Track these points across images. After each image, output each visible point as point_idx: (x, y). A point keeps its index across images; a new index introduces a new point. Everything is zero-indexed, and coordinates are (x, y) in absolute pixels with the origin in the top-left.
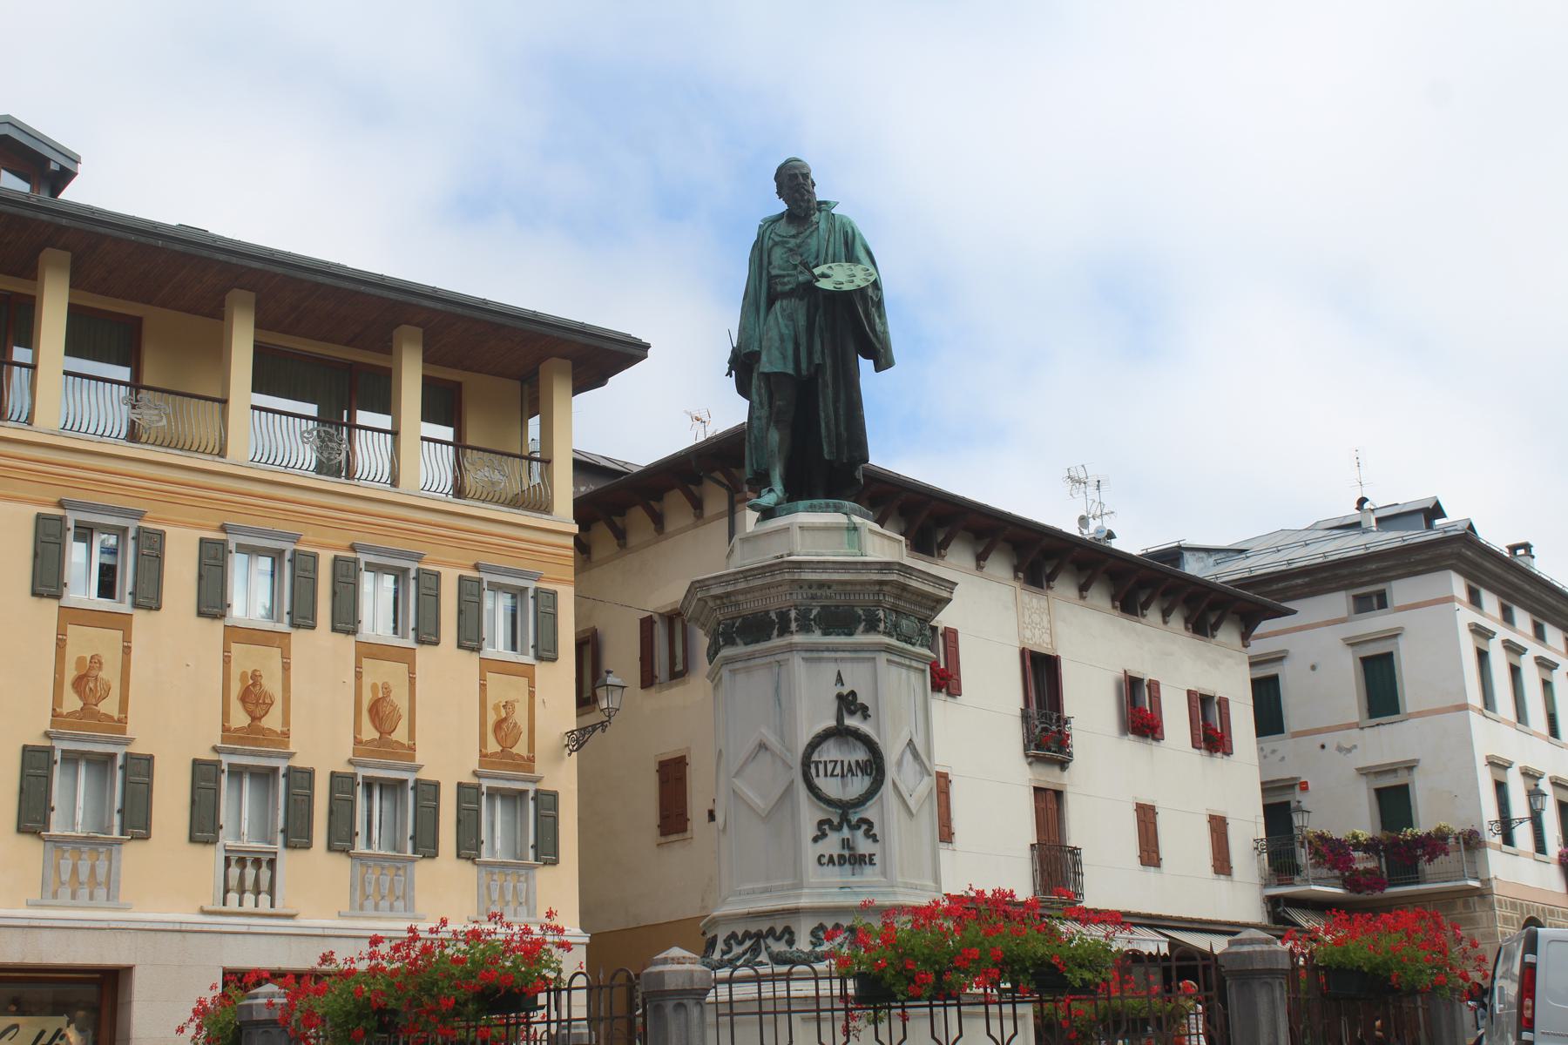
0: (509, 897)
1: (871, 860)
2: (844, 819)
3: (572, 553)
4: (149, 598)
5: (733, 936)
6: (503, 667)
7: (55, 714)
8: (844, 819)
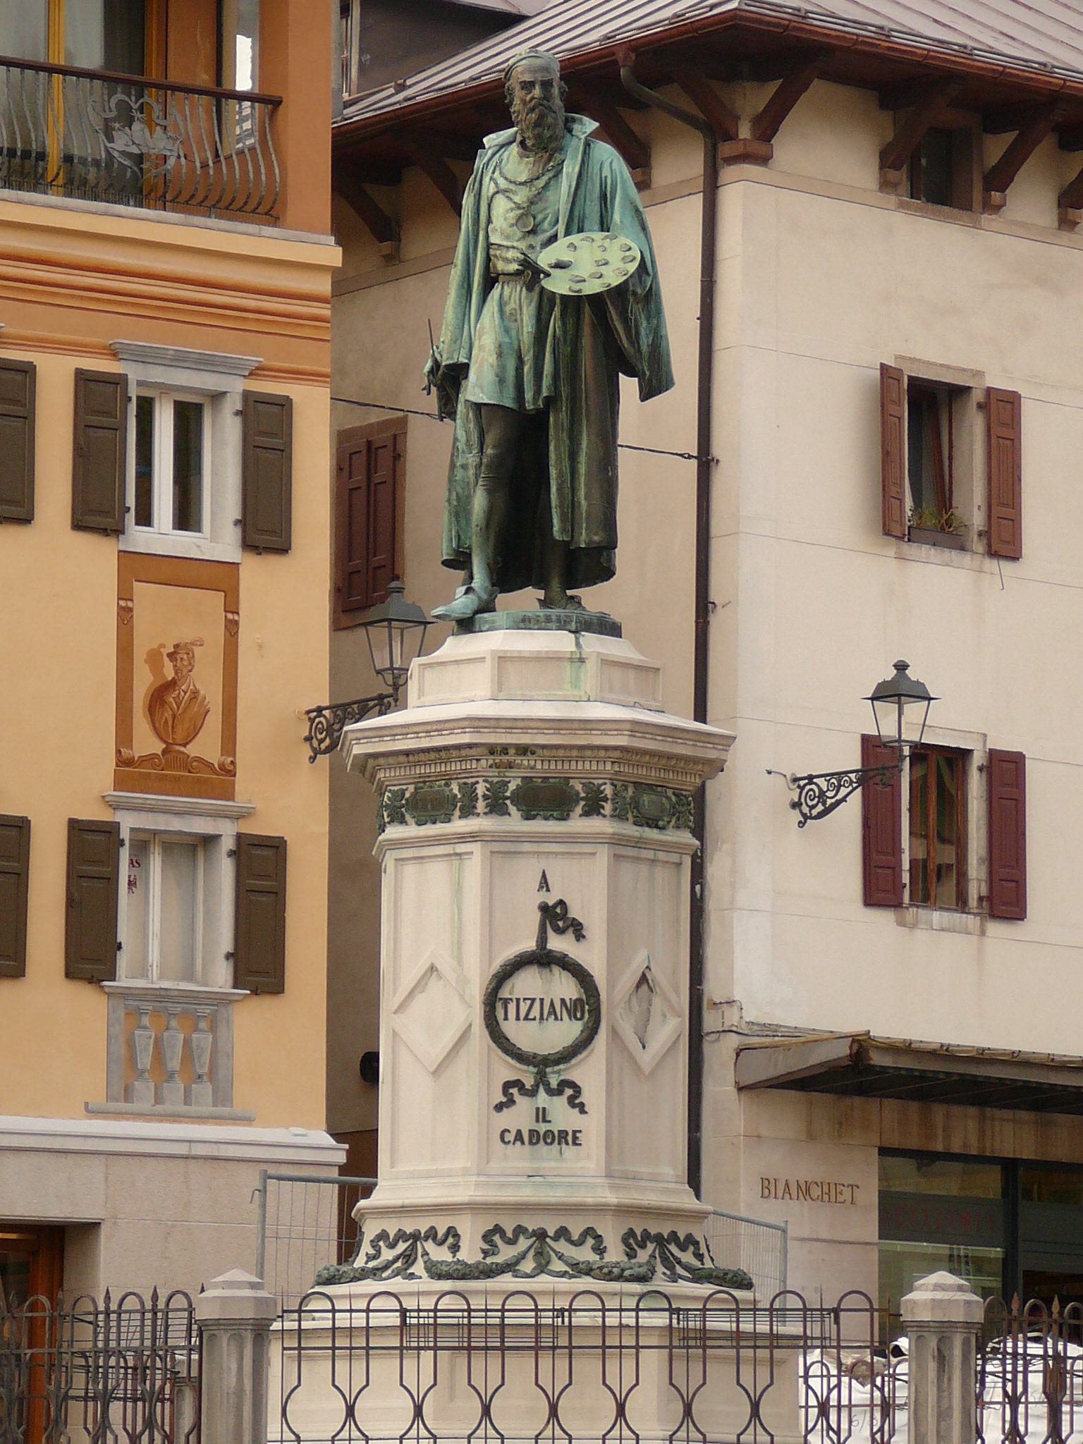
1: (575, 1138)
2: (541, 1079)
5: (383, 1235)
8: (541, 1079)
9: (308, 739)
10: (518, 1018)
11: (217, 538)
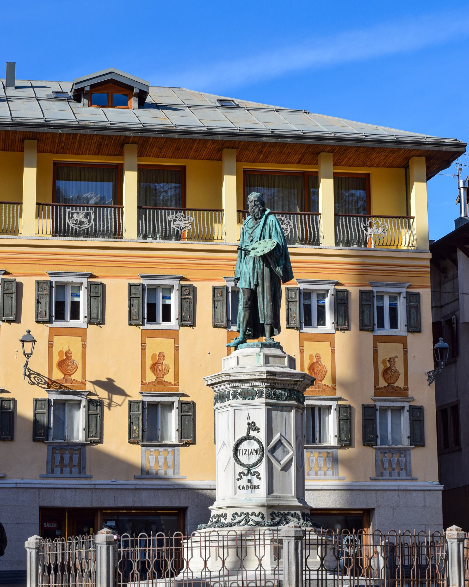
0: (394, 466)
1: (258, 487)
3: (428, 270)
7: (143, 384)
9: (428, 380)
10: (242, 455)
11: (401, 330)
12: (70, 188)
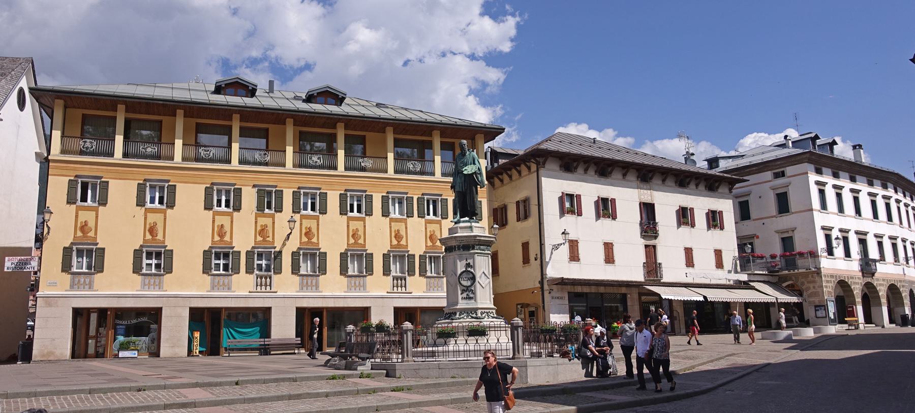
4: (369, 213)
6: (396, 220)
12: (204, 138)
